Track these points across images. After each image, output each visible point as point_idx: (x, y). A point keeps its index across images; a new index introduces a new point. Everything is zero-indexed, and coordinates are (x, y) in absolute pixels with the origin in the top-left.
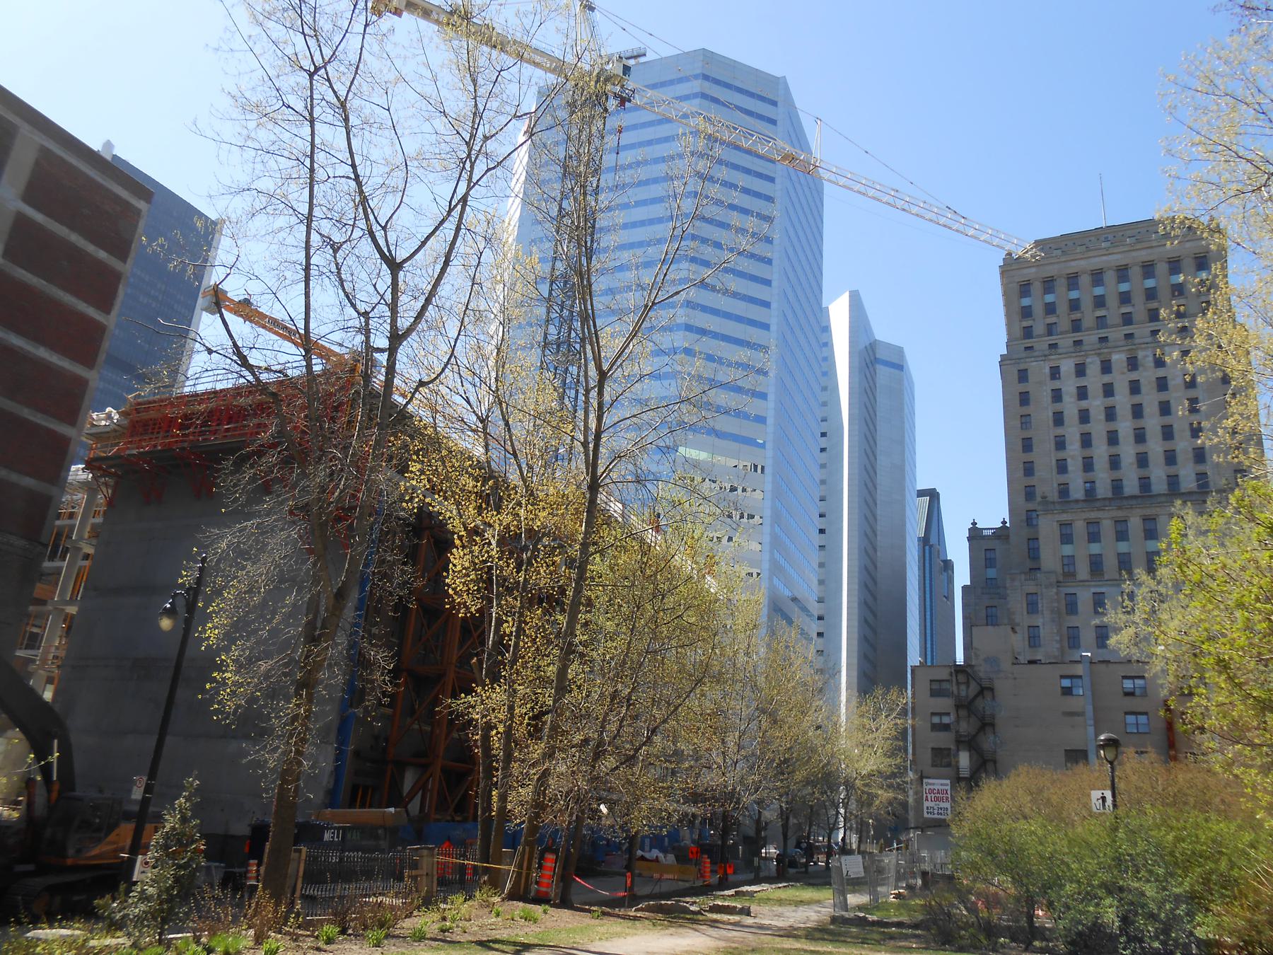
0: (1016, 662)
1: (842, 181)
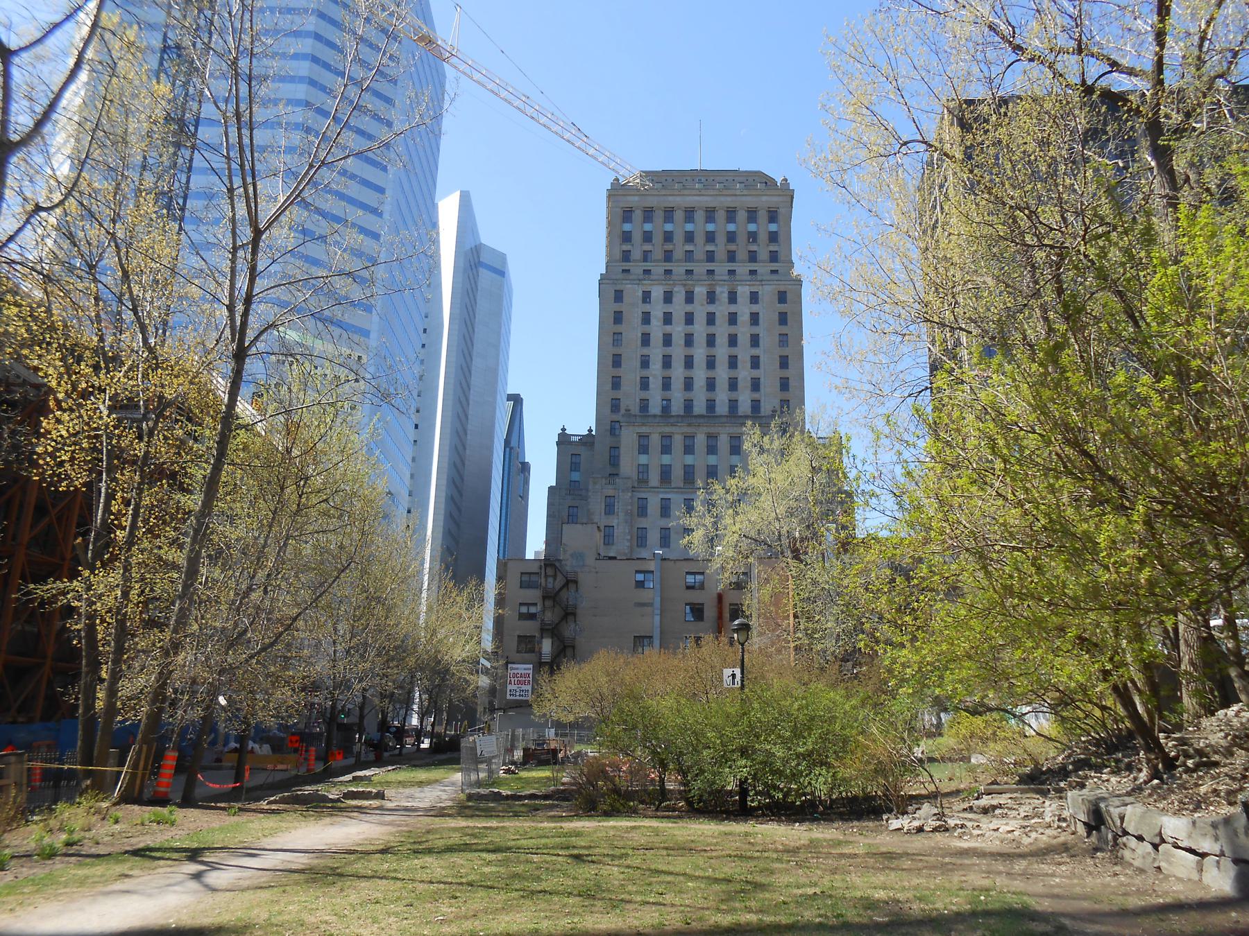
1: (477, 76)
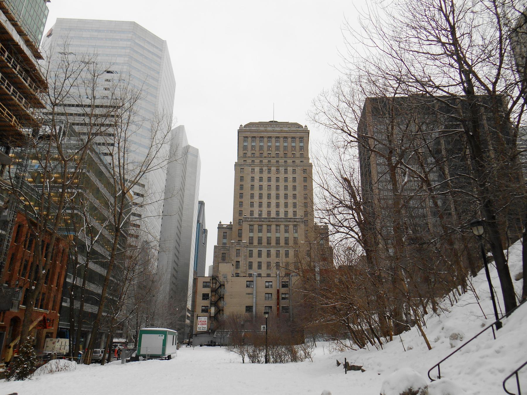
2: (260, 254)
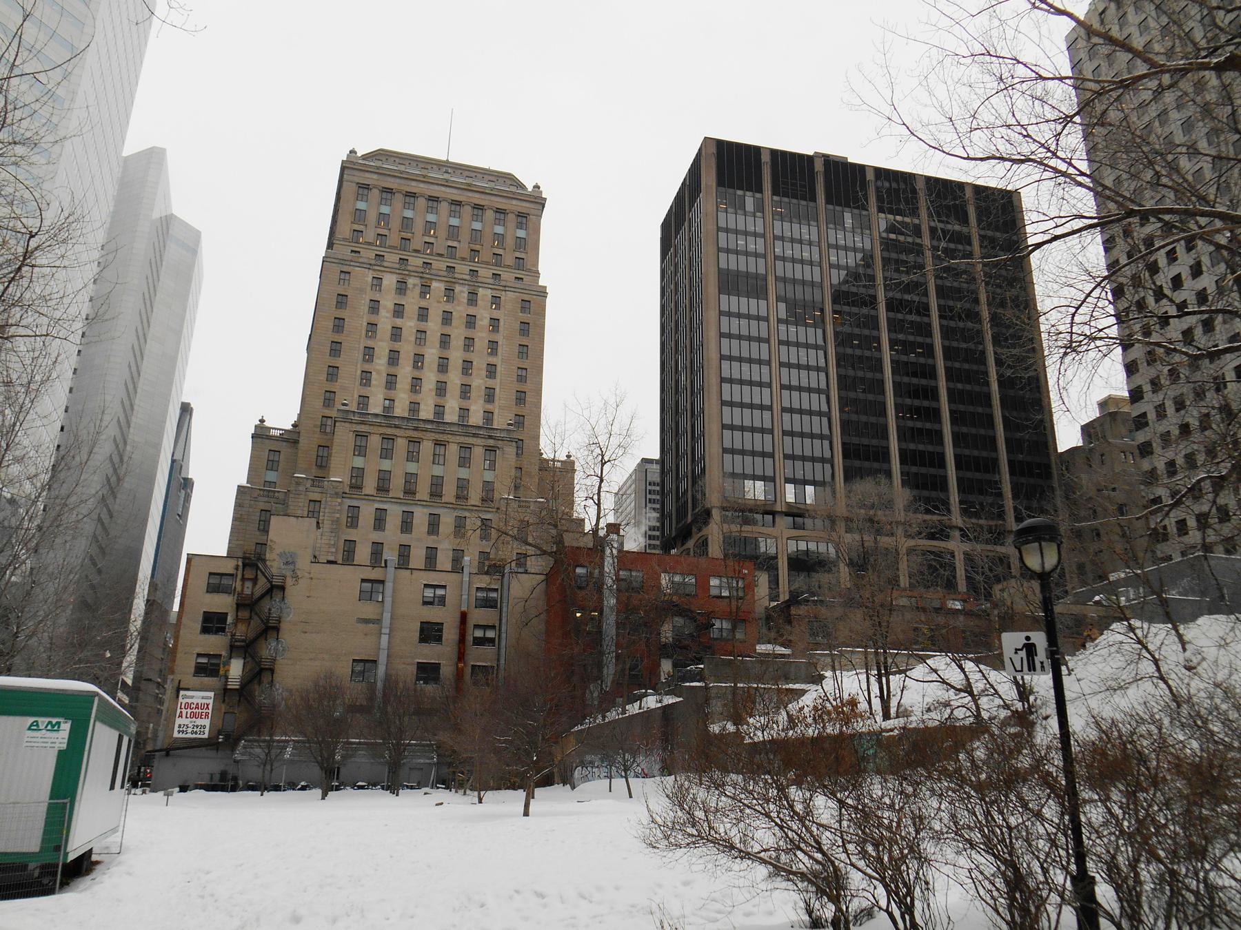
0: (315, 560)
2: (380, 522)
